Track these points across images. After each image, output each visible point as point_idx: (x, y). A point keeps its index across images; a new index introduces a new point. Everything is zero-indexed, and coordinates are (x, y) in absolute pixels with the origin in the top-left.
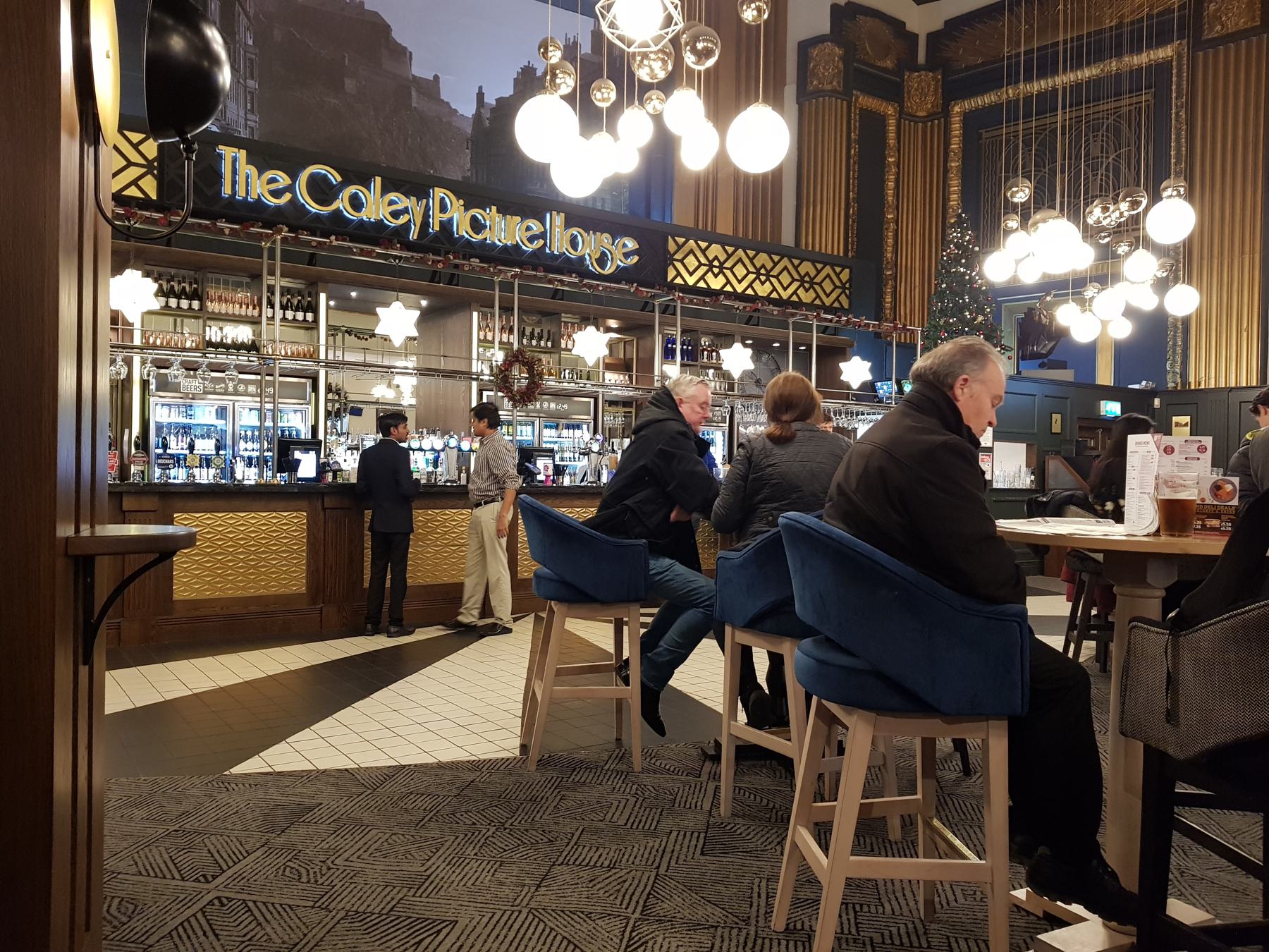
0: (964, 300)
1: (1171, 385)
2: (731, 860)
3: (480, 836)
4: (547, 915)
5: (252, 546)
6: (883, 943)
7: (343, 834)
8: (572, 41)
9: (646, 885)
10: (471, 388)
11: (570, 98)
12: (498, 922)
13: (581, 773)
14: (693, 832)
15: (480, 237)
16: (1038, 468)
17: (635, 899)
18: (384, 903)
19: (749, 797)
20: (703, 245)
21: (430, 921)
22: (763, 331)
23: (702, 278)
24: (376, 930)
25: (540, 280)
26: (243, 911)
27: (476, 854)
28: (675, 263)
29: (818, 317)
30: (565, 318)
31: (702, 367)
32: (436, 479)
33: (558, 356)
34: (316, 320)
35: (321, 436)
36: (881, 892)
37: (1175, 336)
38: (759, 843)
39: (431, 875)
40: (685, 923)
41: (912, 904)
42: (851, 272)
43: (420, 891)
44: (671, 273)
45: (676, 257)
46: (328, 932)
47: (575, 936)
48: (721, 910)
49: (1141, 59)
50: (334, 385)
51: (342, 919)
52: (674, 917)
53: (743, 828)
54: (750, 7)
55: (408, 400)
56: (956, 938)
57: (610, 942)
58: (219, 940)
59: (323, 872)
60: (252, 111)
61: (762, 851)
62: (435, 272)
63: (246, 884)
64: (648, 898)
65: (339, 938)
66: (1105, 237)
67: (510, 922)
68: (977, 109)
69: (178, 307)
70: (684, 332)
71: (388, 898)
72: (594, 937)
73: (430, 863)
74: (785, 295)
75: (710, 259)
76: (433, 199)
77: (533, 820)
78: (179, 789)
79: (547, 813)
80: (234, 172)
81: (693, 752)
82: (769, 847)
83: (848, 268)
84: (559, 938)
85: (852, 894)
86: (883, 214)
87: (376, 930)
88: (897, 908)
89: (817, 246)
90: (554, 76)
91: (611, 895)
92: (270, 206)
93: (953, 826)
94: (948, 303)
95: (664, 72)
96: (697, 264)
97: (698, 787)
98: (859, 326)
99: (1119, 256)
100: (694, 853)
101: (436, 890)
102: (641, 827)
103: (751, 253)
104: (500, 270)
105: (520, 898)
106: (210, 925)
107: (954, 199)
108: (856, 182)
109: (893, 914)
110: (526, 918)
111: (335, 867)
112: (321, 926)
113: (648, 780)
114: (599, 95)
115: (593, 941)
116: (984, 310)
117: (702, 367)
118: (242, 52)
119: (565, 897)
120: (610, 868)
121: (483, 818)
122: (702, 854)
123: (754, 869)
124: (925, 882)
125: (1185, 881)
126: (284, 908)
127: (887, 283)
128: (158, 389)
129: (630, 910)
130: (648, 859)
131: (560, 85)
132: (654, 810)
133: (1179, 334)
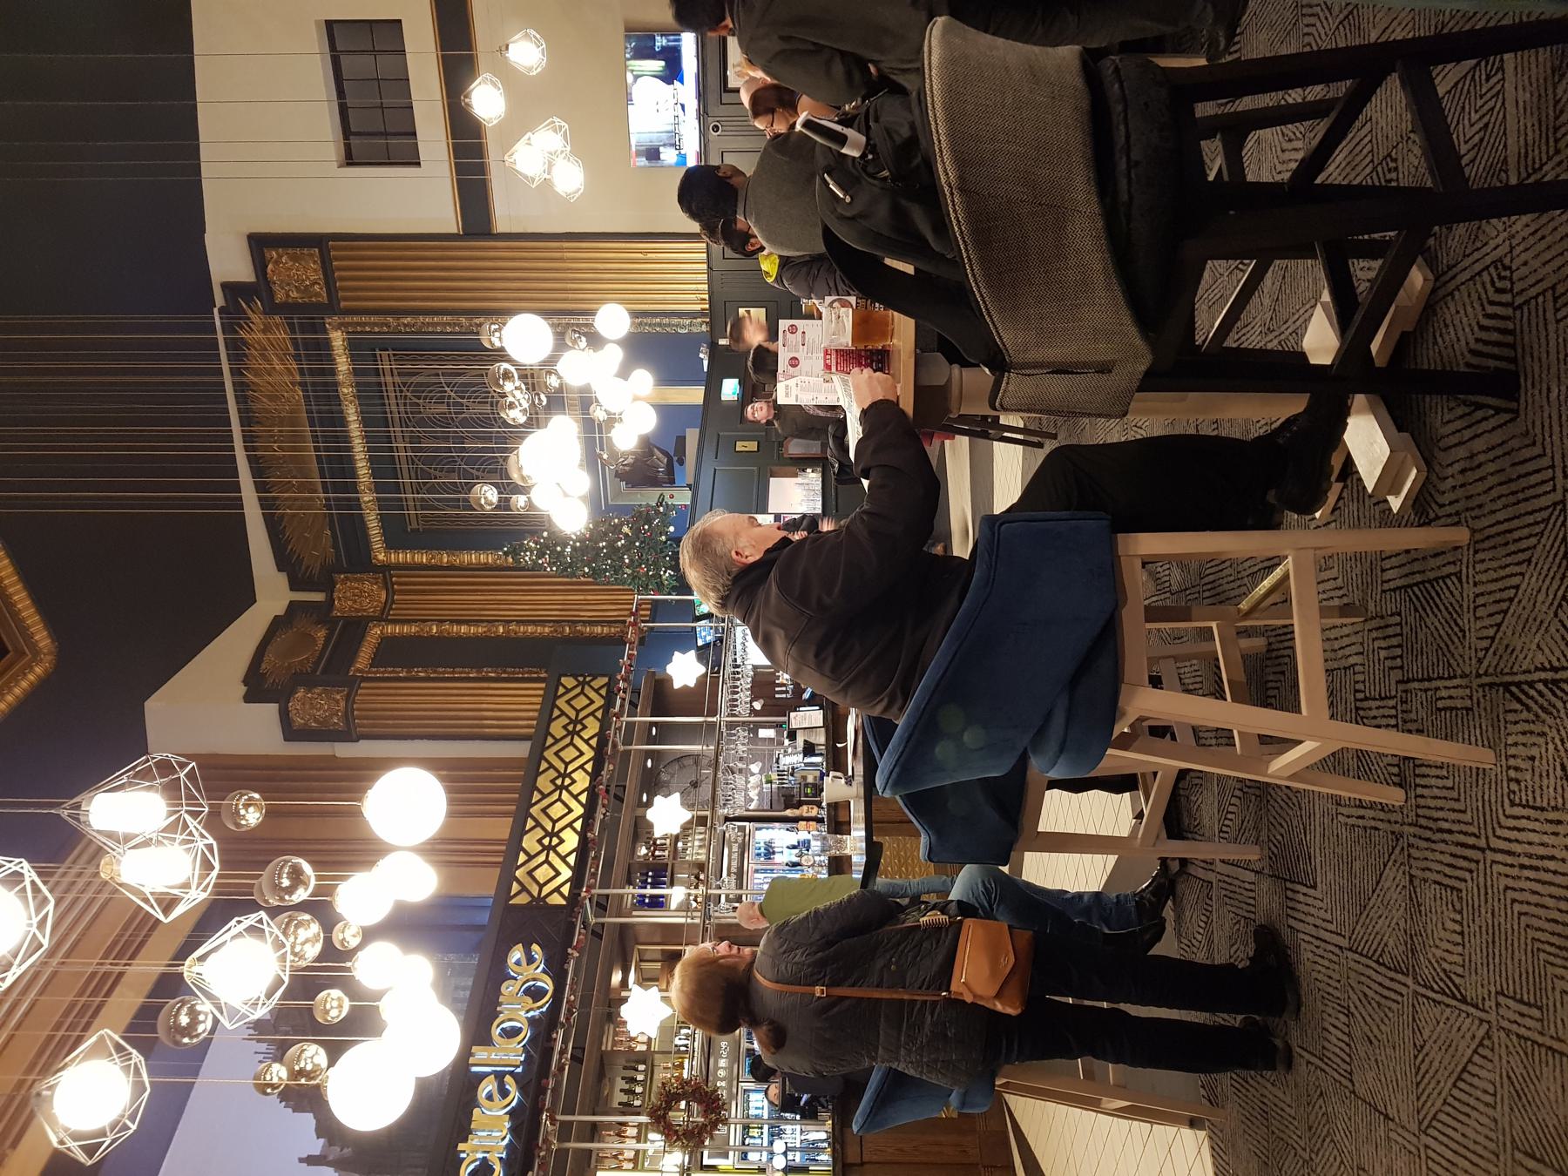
0: (604, 547)
1: (704, 328)
2: (1318, 851)
6: (1402, 668)
8: (252, 1032)
9: (1367, 966)
11: (335, 1052)
14: (1287, 898)
16: (800, 464)
17: (1387, 983)
19: (1231, 820)
20: (522, 858)
22: (632, 782)
23: (563, 859)
25: (558, 1083)
28: (543, 894)
29: (618, 716)
30: (607, 1045)
31: (674, 858)
33: (656, 1056)
37: (650, 325)
42: (566, 675)
44: (556, 900)
45: (536, 894)
47: (1450, 1068)
49: (343, 364)
52: (1405, 931)
53: (1274, 832)
54: (244, 816)
56: (1383, 582)
57: (1452, 1020)
61: (1301, 809)
64: (1383, 964)
66: (539, 399)
67: (1444, 1163)
70: (630, 882)
74: (589, 754)
75: (541, 848)
77: (1294, 1118)
84: (1455, 1092)
88: (1354, 649)
89: (531, 714)
91: (1386, 1015)
93: (1240, 576)
94: (606, 565)
95: (312, 925)
96: (546, 866)
99: (561, 385)
100: (1315, 898)
104: (544, 1141)
107: (486, 558)
108: (457, 670)
109: (1362, 653)
110: (1436, 1139)
114: (334, 1013)
115: (1454, 1045)
117: (674, 858)
119: (1397, 1080)
120: (1349, 1014)
122: (1314, 887)
125: (1279, 328)
129: (1404, 990)
130: (1330, 961)
131: (315, 1065)
133: (648, 320)
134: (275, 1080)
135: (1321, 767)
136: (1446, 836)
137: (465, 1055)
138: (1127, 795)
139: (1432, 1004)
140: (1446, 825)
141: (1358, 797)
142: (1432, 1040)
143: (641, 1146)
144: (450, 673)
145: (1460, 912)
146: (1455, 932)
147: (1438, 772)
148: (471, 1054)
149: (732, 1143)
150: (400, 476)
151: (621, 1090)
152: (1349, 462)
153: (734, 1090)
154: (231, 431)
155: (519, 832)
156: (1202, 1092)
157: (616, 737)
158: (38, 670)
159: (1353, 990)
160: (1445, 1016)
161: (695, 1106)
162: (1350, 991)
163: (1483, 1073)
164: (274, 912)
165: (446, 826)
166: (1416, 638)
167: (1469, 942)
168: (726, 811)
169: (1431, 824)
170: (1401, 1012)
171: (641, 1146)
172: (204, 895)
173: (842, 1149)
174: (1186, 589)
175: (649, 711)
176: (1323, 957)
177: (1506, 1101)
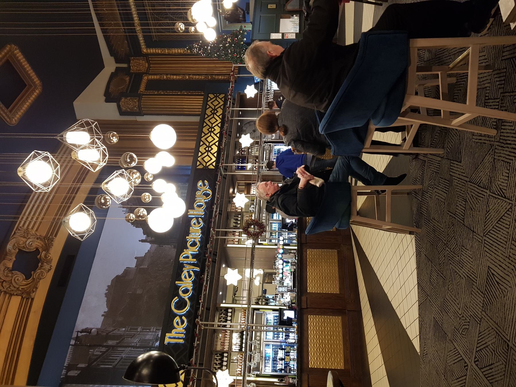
0: (221, 46)
2: (464, 150)
3: (450, 254)
4: (487, 229)
5: (322, 337)
6: (503, 88)
7: (448, 310)
9: (474, 187)
10: (258, 248)
11: (149, 211)
12: (489, 250)
13: (423, 210)
14: (451, 166)
15: (198, 243)
16: (290, 14)
17: (480, 192)
18: (479, 296)
19: (435, 141)
20: (200, 154)
21: (488, 277)
22: (234, 130)
24: (491, 300)
25: (215, 220)
26: (481, 353)
27: (458, 256)
28: (207, 165)
29: (229, 107)
31: (248, 155)
32: (294, 262)
33: (244, 213)
34: (231, 308)
35: (278, 308)
36: (480, 88)
38: (456, 138)
39: (467, 275)
40: (492, 172)
41: (485, 75)
42: (210, 94)
43: (474, 280)
44: (211, 167)
45: (205, 165)
46: (491, 319)
47: (496, 218)
48: (487, 156)
50: (256, 301)
51: (486, 313)
53: (449, 144)
55: (261, 272)
57: (500, 204)
58: (494, 364)
59: (465, 319)
60: (150, 329)
62: (213, 261)
63: (469, 350)
64: (480, 186)
65: (494, 315)
68: (145, 42)
69: (226, 361)
70: (234, 162)
71: (477, 294)
72: (497, 210)
73: (462, 276)
74: (219, 121)
76: (184, 261)
77: (443, 232)
78: (426, 373)
79: (440, 225)
80: (174, 338)
81: (414, 163)
82: (458, 134)
83: (208, 95)
84: (497, 225)
85: (481, 100)
86: (187, 80)
87: (491, 300)
89: (199, 107)
90: (140, 216)
91: (478, 202)
92: (187, 325)
93: (450, 55)
96: (207, 157)
97: (430, 162)
98: (232, 90)
100: (460, 166)
101: (474, 274)
102: (448, 187)
103: (203, 135)
105: (479, 239)
106: (487, 366)
107: (180, 51)
109: (490, 83)
110: (488, 238)
111: (462, 314)
112: (488, 322)
113: (427, 183)
114: (147, 199)
116: (225, 38)
117: (248, 155)
118: (127, 332)
119: (479, 221)
120: (466, 201)
121: (442, 252)
122: (461, 162)
123: (468, 141)
124: (479, 70)
126: (480, 336)
127: (214, 78)
128: (259, 371)
129: (485, 194)
131: (143, 214)
132: (440, 181)
134: (132, 218)
135: (469, 123)
136: (509, 146)
137: (187, 212)
138: (400, 133)
139: (494, 198)
140: (509, 142)
141: (480, 132)
142: (492, 209)
143: (240, 238)
144: (171, 92)
145: (509, 170)
146: (506, 176)
147: (510, 124)
148: (188, 212)
149: (267, 237)
150: (149, 20)
151: (234, 222)
152: (498, 9)
153: (268, 223)
154: (88, 3)
155: (198, 146)
156: (415, 224)
157: (228, 115)
158: (37, 91)
159: (468, 194)
160: (498, 202)
161: (256, 227)
162: (467, 194)
163: (507, 219)
164: (126, 169)
165: (177, 143)
166: (511, 77)
167: (510, 179)
168: (265, 140)
169: (504, 142)
170: (483, 201)
171: (240, 238)
172: (105, 164)
173: (300, 239)
174: (430, 60)
175: (239, 106)
176: (460, 184)
177: (513, 227)
